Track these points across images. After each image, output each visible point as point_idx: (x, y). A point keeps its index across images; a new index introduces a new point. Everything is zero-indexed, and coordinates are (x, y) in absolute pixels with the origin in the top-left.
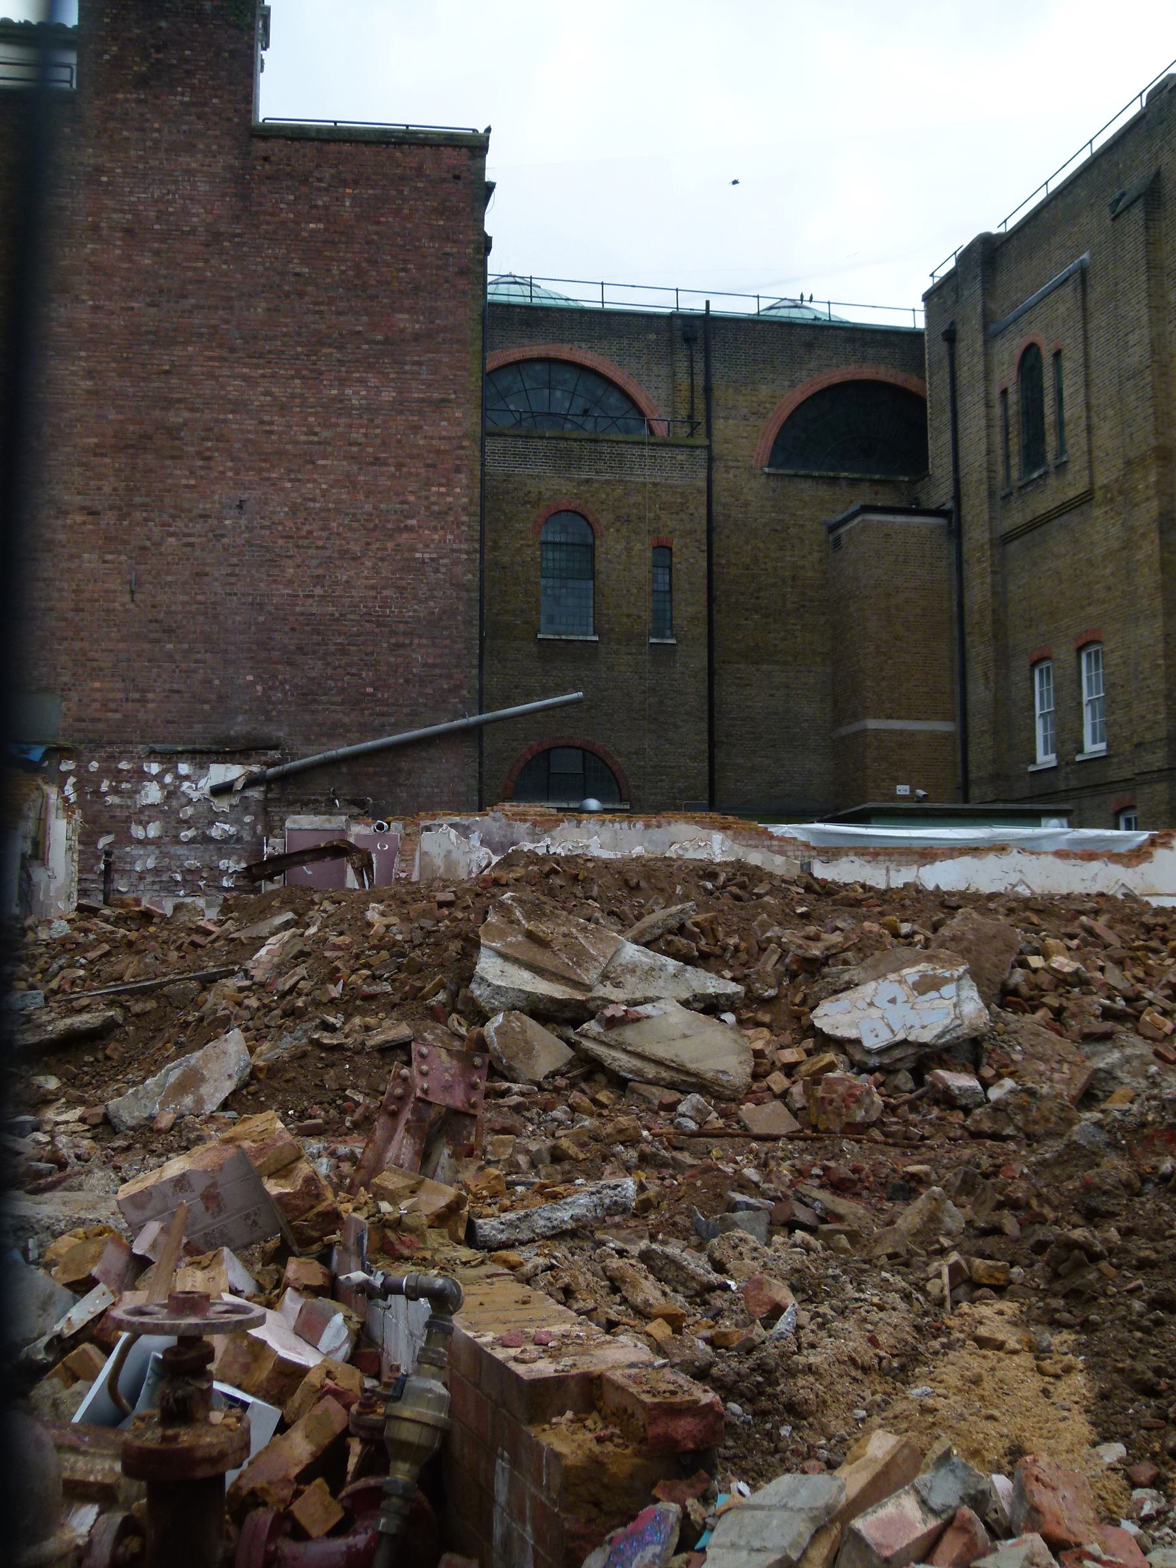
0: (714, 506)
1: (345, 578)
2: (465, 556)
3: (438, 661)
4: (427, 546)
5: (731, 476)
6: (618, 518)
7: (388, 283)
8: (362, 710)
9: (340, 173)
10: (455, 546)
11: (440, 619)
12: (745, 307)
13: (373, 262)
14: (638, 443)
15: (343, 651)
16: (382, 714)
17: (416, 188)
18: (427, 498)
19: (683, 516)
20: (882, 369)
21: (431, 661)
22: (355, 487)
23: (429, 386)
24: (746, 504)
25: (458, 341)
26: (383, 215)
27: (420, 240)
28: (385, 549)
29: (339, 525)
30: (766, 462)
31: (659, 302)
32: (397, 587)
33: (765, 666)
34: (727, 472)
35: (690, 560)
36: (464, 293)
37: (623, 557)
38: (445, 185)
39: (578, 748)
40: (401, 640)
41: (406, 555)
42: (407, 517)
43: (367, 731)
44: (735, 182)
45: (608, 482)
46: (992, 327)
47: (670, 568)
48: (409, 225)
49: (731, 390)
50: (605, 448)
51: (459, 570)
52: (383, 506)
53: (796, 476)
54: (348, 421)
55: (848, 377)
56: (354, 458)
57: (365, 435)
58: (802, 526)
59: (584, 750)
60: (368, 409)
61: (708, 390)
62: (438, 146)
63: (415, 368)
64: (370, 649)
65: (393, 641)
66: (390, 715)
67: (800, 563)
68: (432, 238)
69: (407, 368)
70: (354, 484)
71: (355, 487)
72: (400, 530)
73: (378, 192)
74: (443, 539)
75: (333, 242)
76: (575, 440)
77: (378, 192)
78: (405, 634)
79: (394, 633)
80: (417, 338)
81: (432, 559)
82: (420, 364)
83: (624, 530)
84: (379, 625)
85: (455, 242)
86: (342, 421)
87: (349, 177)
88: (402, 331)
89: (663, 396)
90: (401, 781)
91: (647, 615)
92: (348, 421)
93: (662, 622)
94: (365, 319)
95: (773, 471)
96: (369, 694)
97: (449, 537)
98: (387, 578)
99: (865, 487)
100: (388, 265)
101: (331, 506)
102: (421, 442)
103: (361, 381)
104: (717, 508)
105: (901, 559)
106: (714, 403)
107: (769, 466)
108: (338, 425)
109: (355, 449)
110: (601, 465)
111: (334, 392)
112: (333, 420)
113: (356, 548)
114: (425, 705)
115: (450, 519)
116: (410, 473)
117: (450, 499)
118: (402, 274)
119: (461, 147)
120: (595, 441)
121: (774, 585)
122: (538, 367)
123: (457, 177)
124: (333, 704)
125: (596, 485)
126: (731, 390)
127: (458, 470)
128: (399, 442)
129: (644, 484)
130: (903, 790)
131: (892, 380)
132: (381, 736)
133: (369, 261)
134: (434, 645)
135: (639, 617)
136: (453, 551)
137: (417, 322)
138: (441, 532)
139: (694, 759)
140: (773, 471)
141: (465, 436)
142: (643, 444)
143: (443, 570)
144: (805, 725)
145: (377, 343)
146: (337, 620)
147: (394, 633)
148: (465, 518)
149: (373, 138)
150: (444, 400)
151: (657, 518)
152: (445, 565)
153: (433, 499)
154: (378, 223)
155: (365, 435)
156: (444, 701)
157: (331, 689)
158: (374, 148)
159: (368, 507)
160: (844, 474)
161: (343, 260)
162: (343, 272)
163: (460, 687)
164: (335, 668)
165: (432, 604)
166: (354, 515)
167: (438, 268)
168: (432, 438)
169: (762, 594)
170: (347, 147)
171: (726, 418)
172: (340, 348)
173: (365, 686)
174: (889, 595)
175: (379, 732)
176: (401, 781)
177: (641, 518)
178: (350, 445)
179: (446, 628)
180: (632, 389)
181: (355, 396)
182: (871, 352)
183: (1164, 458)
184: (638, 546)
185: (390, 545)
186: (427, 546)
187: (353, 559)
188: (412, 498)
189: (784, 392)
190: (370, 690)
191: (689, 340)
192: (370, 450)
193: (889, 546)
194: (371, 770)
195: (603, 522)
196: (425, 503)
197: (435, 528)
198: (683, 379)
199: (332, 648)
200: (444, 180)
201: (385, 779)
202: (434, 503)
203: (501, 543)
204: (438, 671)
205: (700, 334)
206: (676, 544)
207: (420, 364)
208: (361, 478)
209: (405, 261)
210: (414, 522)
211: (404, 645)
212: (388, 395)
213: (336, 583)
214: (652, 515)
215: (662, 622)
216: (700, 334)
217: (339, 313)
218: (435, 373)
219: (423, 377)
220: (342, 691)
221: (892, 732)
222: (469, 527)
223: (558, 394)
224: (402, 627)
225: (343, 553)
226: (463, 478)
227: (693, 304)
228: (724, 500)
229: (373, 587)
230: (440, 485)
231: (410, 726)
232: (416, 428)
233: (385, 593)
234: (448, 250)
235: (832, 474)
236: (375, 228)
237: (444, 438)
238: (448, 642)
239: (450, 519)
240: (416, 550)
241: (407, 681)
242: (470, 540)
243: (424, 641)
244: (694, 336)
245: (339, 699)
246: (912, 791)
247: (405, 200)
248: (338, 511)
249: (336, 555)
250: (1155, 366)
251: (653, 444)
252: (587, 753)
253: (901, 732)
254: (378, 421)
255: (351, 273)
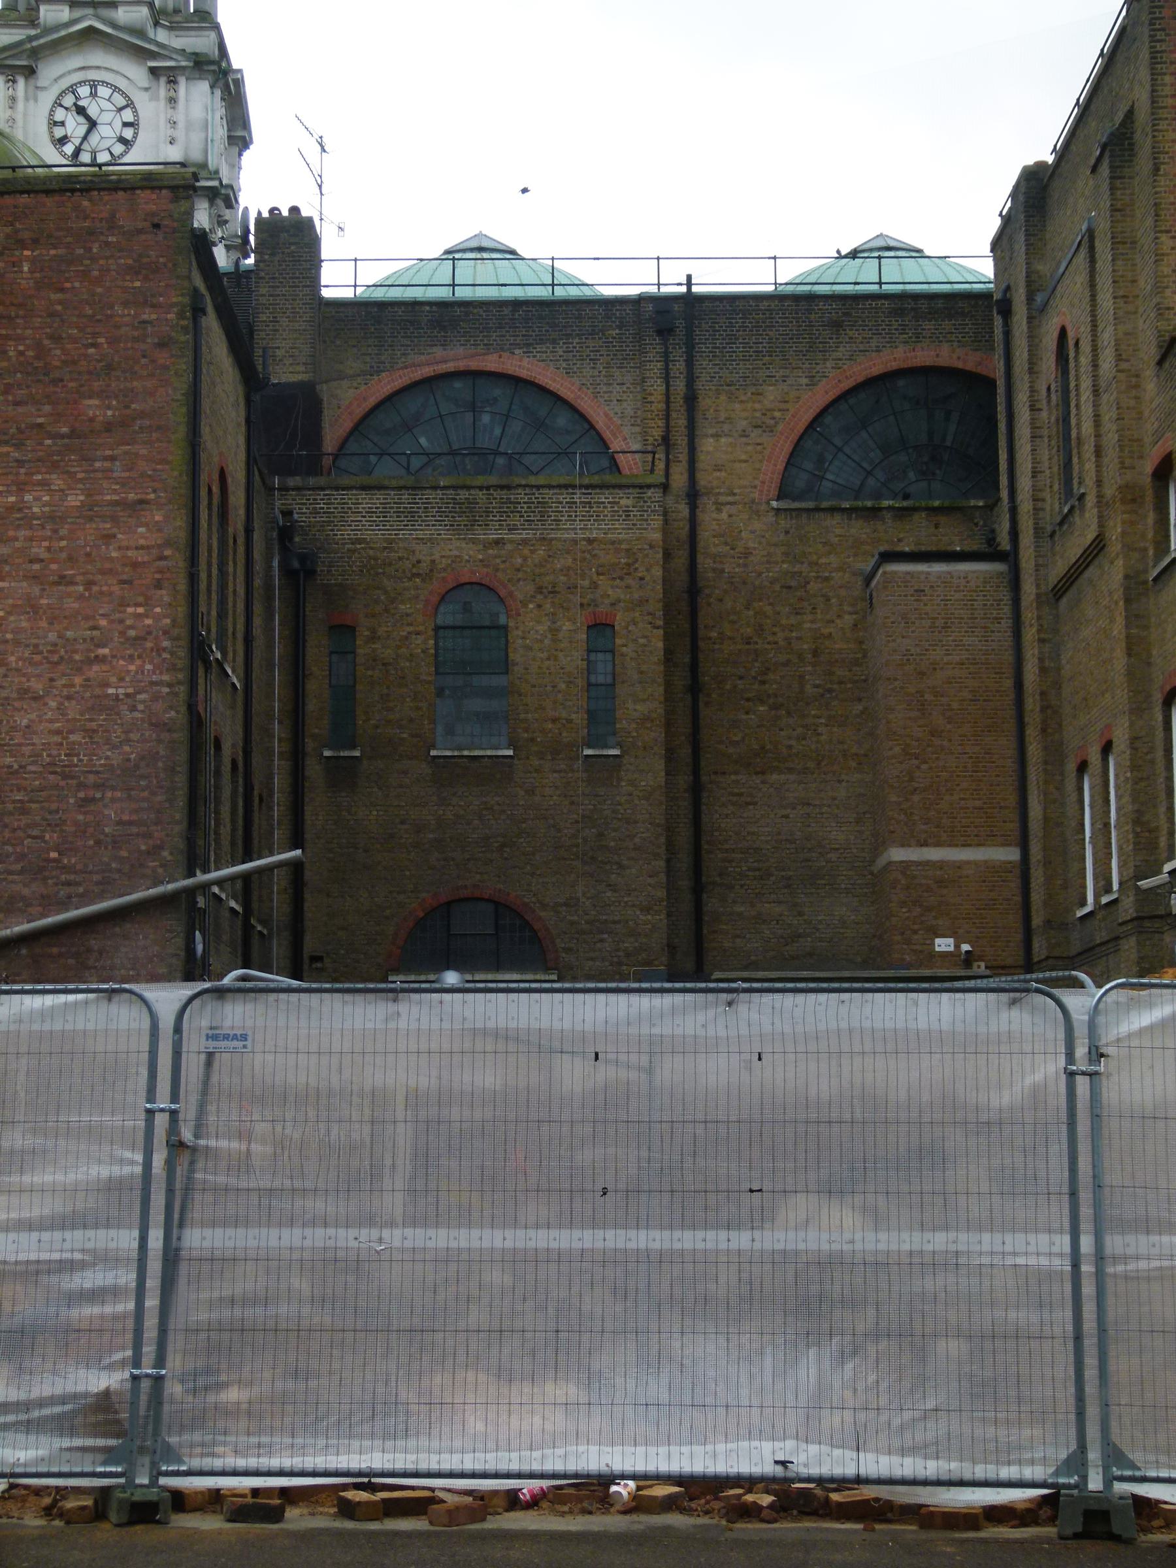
0: (700, 558)
1: (25, 722)
2: (166, 690)
3: (134, 817)
4: (122, 679)
5: (724, 516)
6: (540, 590)
7: (74, 362)
8: (45, 879)
9: (17, 231)
10: (154, 678)
11: (137, 767)
12: (753, 277)
13: (56, 338)
14: (566, 487)
15: (24, 811)
16: (68, 884)
17: (107, 244)
18: (121, 621)
19: (629, 581)
20: (945, 349)
21: (126, 818)
22: (36, 613)
23: (123, 485)
24: (747, 554)
25: (159, 428)
26: (67, 280)
27: (112, 308)
28: (73, 686)
29: (20, 659)
30: (774, 492)
31: (619, 278)
32: (85, 731)
33: (775, 776)
34: (719, 510)
35: (642, 642)
36: (166, 368)
37: (545, 645)
38: (143, 237)
39: (489, 900)
40: (91, 793)
41: (98, 691)
42: (98, 646)
43: (49, 903)
44: (525, 191)
45: (525, 542)
46: (1039, 298)
47: (612, 652)
48: (99, 290)
49: (723, 398)
50: (521, 495)
51: (158, 706)
52: (69, 634)
53: (818, 509)
54: (28, 533)
55: (894, 366)
56: (35, 578)
57: (49, 549)
58: (827, 579)
59: (496, 904)
60: (51, 518)
61: (691, 399)
62: (134, 189)
63: (107, 464)
64: (54, 806)
65: (81, 795)
66: (78, 884)
67: (826, 631)
68: (125, 304)
69: (98, 464)
70: (35, 608)
71: (36, 613)
72: (90, 662)
73: (61, 251)
74: (141, 670)
75: (10, 318)
76: (481, 488)
77: (61, 251)
78: (97, 786)
79: (81, 786)
80: (109, 427)
81: (127, 695)
82: (112, 459)
83: (548, 607)
84: (65, 777)
85: (153, 306)
86: (22, 533)
87: (26, 235)
88: (92, 420)
89: (630, 411)
90: (91, 962)
91: (579, 718)
92: (28, 533)
93: (601, 721)
94: (47, 408)
95: (783, 504)
96: (55, 860)
97: (148, 667)
98: (75, 720)
99: (920, 518)
100: (74, 340)
101: (9, 636)
102: (114, 554)
103: (44, 484)
104: (704, 563)
105: (940, 623)
106: (699, 416)
107: (779, 498)
108: (16, 539)
109: (36, 567)
110: (515, 520)
111: (12, 499)
112: (11, 533)
113: (38, 686)
114: (119, 871)
115: (149, 645)
116: (101, 593)
117: (148, 622)
118: (92, 351)
119: (160, 188)
120: (508, 487)
121: (787, 663)
122: (458, 384)
123: (157, 226)
124: (10, 873)
125: (509, 547)
126: (723, 398)
127: (158, 585)
128: (88, 555)
129: (575, 542)
130: (944, 944)
131: (960, 365)
132: (67, 910)
133: (51, 337)
134: (129, 797)
135: (570, 721)
136: (152, 683)
137: (109, 408)
138: (138, 662)
139: (647, 910)
140: (783, 504)
141: (168, 543)
142: (574, 487)
143: (141, 707)
144: (833, 856)
145: (63, 436)
146: (17, 772)
147: (81, 786)
148: (166, 644)
149: (55, 186)
150: (141, 502)
151: (594, 585)
152: (143, 702)
153: (128, 622)
154: (62, 290)
155: (49, 549)
156: (141, 865)
157: (8, 856)
158: (57, 198)
159: (52, 636)
160: (886, 503)
161: (20, 339)
162: (21, 353)
163: (161, 847)
164: (14, 830)
165: (127, 749)
166: (36, 646)
167: (136, 339)
168: (128, 548)
169: (771, 676)
170: (24, 199)
171: (716, 436)
172: (19, 446)
173: (48, 850)
174: (922, 674)
175: (64, 905)
176: (91, 962)
177: (572, 588)
178: (31, 562)
179: (142, 777)
180: (586, 404)
181: (36, 502)
182: (928, 326)
183: (1134, 501)
184: (567, 626)
185: (78, 680)
186: (122, 679)
187: (35, 699)
188: (103, 623)
189: (798, 395)
190: (54, 855)
191: (665, 332)
192: (54, 567)
193: (935, 604)
194: (55, 950)
195: (519, 596)
196: (120, 628)
197: (131, 657)
198: (657, 388)
199: (10, 807)
200: (140, 231)
201: (71, 961)
202: (131, 627)
203: (381, 631)
204: (135, 830)
205: (680, 323)
206: (620, 620)
207: (112, 459)
208: (44, 601)
209: (95, 335)
210: (106, 651)
211: (93, 800)
212: (75, 500)
213: (14, 728)
214: (586, 583)
215: (601, 721)
216: (680, 323)
217: (17, 404)
218: (130, 470)
219: (115, 475)
220: (21, 857)
221: (928, 863)
222: (172, 653)
223: (486, 418)
224: (92, 778)
225: (24, 693)
226: (165, 595)
227: (672, 281)
228: (713, 550)
229: (58, 732)
230: (137, 605)
231: (101, 897)
232: (109, 538)
233: (73, 738)
234: (145, 317)
235: (869, 504)
236: (60, 296)
237: (142, 548)
238: (146, 794)
239: (149, 645)
240: (108, 685)
241: (98, 843)
242: (173, 668)
243: (119, 794)
244: (677, 326)
245: (18, 867)
246: (957, 946)
247: (93, 259)
248: (17, 643)
249: (14, 695)
250: (1121, 376)
251: (587, 487)
252: (500, 907)
253: (941, 865)
254: (63, 532)
255: (31, 353)
